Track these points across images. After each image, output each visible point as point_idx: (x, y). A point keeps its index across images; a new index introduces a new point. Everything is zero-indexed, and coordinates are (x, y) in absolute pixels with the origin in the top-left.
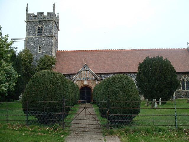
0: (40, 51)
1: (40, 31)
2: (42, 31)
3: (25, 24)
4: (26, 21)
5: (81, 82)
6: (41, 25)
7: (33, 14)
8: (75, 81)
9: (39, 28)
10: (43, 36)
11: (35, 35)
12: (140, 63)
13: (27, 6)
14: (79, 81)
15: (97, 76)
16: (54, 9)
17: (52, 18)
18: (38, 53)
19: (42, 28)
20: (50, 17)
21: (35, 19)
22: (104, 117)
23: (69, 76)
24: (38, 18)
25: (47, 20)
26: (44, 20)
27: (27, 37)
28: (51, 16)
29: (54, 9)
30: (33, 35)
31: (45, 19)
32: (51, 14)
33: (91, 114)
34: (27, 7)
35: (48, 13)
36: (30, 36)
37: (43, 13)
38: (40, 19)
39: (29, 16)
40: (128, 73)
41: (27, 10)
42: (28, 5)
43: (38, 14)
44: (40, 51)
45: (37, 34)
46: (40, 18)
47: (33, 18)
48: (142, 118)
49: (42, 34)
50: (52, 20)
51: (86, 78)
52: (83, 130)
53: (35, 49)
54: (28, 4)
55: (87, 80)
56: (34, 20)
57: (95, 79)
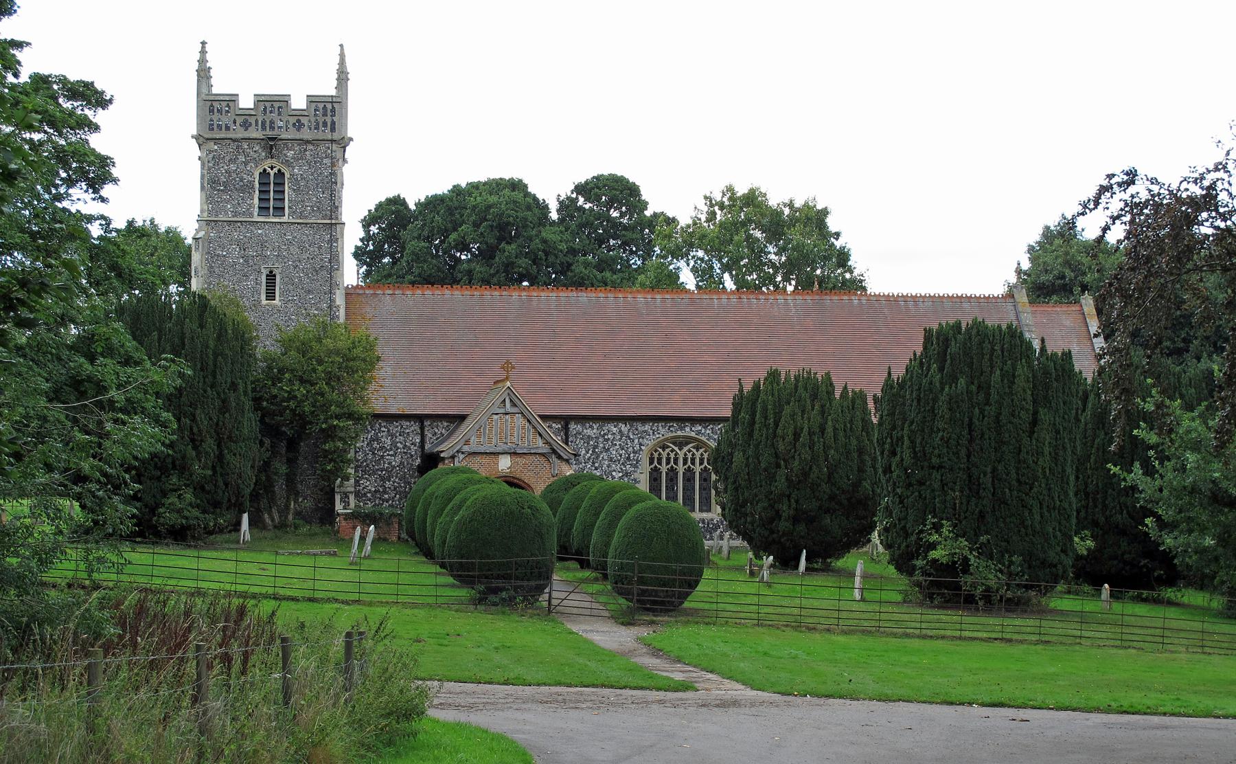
0: (271, 295)
1: (271, 189)
2: (283, 192)
3: (194, 151)
4: (201, 140)
5: (485, 460)
6: (274, 162)
7: (232, 99)
8: (461, 456)
9: (264, 174)
10: (285, 219)
11: (251, 215)
12: (748, 388)
13: (203, 52)
14: (478, 459)
15: (553, 432)
16: (342, 77)
17: (333, 129)
18: (264, 302)
19: (280, 174)
20: (325, 124)
21: (246, 125)
22: (621, 593)
23: (416, 427)
24: (263, 123)
25: (306, 134)
26: (291, 134)
27: (208, 222)
28: (329, 120)
29: (342, 77)
30: (235, 214)
31: (298, 130)
32: (329, 106)
33: (571, 592)
34: (202, 61)
35: (311, 100)
36: (221, 217)
37: (283, 101)
38: (272, 128)
39: (212, 111)
40: (693, 420)
41: (204, 73)
42: (208, 47)
43: (260, 100)
44: (271, 295)
45: (256, 214)
46: (272, 122)
47: (235, 122)
48: (692, 605)
49: (280, 210)
50: (332, 141)
51: (505, 447)
52: (588, 612)
53: (251, 283)
54: (203, 43)
55: (514, 454)
56: (240, 136)
57: (546, 449)
